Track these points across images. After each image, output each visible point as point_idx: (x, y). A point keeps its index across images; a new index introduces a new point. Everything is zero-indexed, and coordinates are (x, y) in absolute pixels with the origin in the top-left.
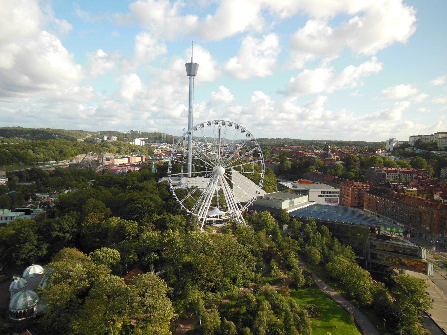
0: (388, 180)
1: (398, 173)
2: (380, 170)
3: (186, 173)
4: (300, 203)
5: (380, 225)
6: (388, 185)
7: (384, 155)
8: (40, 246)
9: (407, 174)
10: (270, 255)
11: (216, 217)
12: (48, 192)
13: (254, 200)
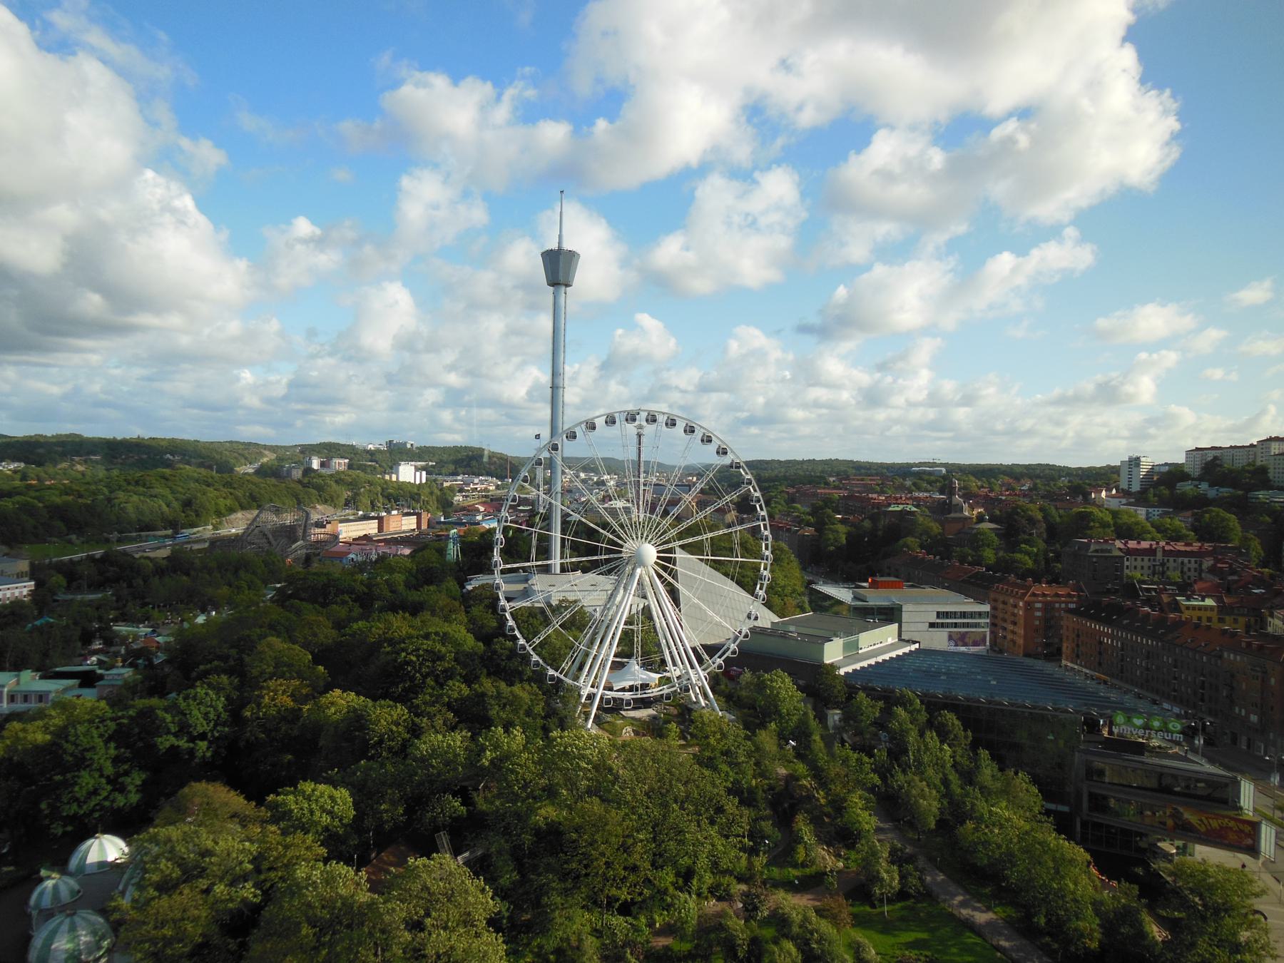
1: (1159, 555)
2: (1105, 547)
3: (545, 562)
5: (1114, 709)
6: (1130, 590)
7: (1114, 504)
9: (1186, 560)
11: (631, 689)
13: (741, 638)
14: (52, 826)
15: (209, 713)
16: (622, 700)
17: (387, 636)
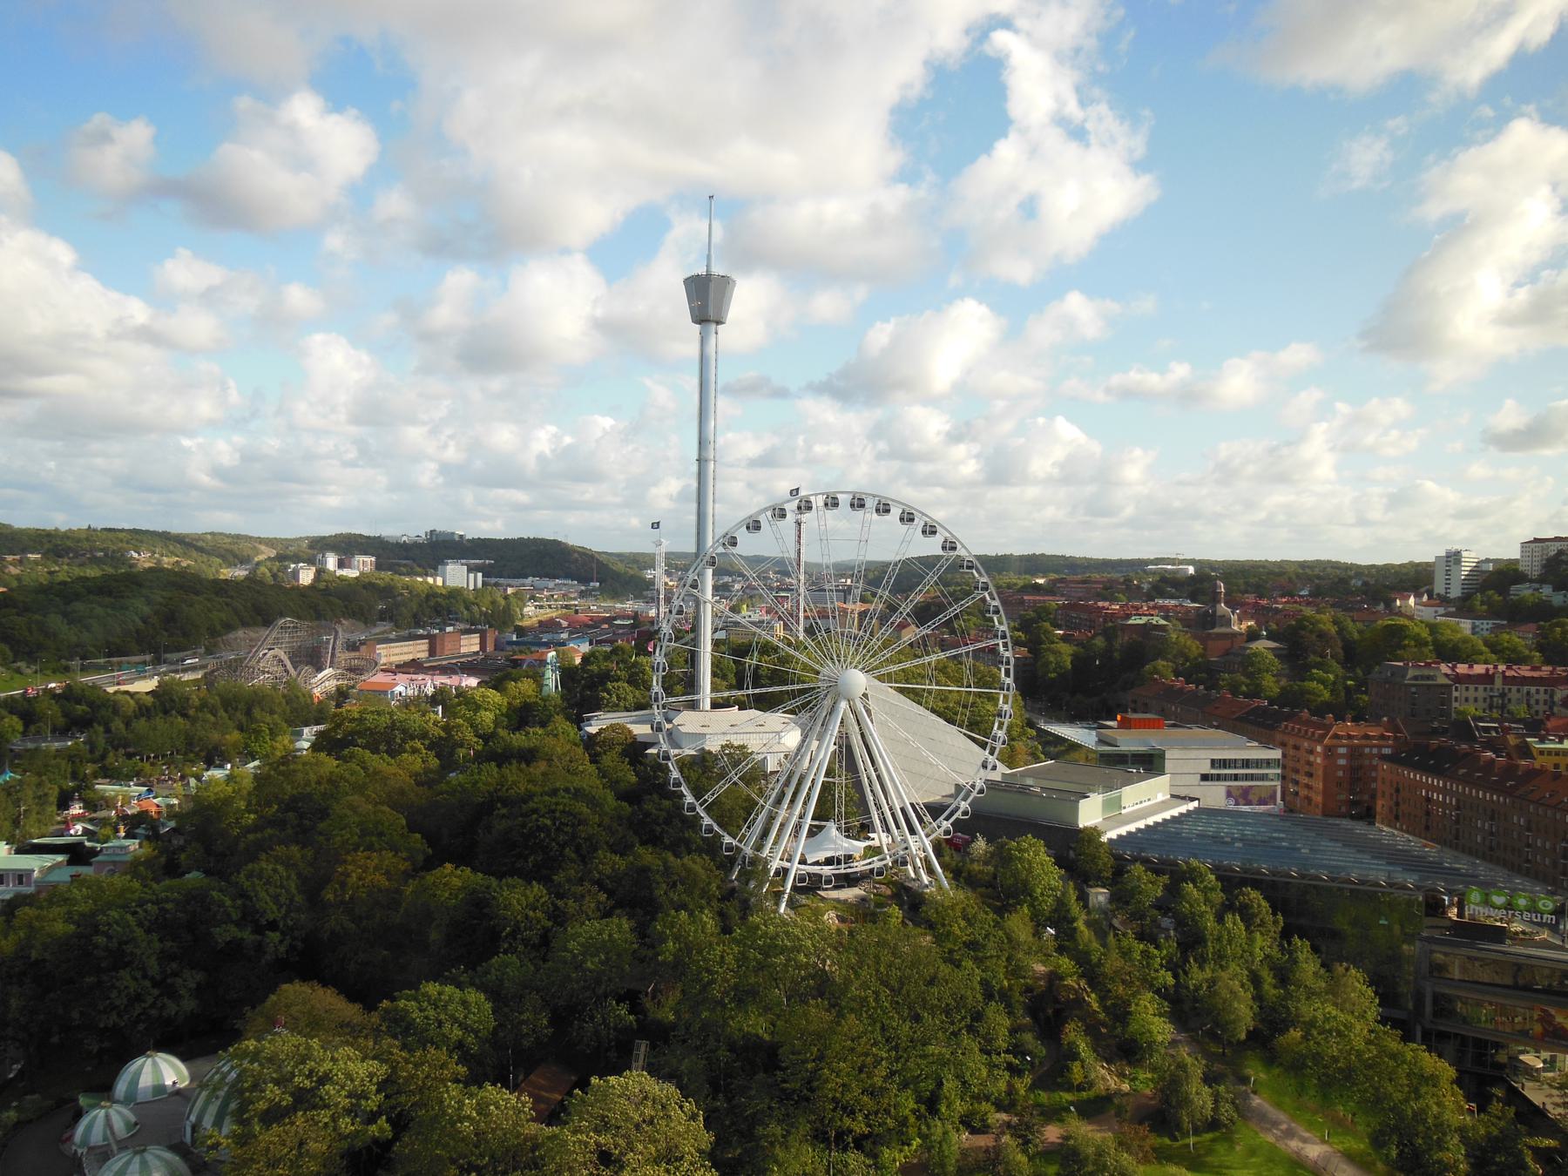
0: (1458, 712)
1: (1498, 682)
2: (1426, 672)
3: (689, 698)
4: (1144, 805)
5: (1467, 884)
6: (1463, 729)
7: (1428, 614)
8: (169, 981)
9: (1533, 689)
10: (1058, 1006)
11: (829, 862)
12: (138, 774)
13: (974, 794)
14: (85, 1041)
15: (279, 895)
16: (821, 876)
17: (500, 794)
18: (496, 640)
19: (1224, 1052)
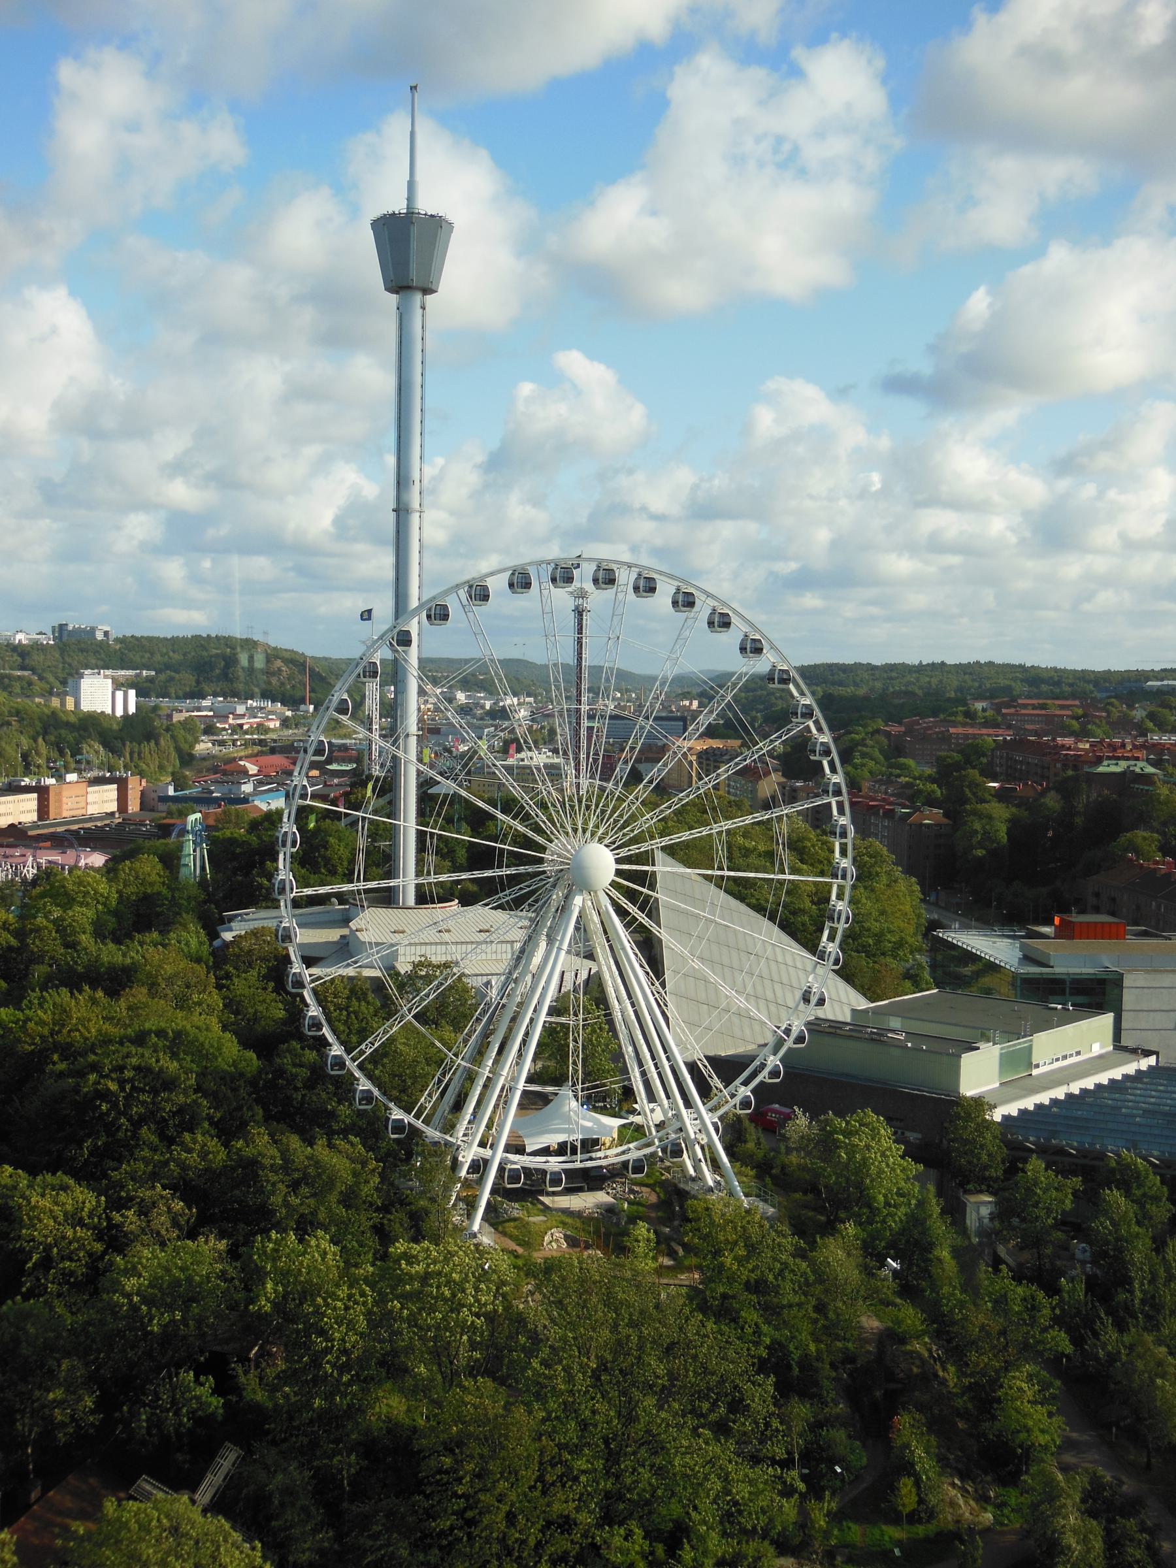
3: (384, 884)
11: (562, 1150)
13: (789, 1043)
17: (58, 1038)
18: (143, 793)
19: (1149, 1463)
